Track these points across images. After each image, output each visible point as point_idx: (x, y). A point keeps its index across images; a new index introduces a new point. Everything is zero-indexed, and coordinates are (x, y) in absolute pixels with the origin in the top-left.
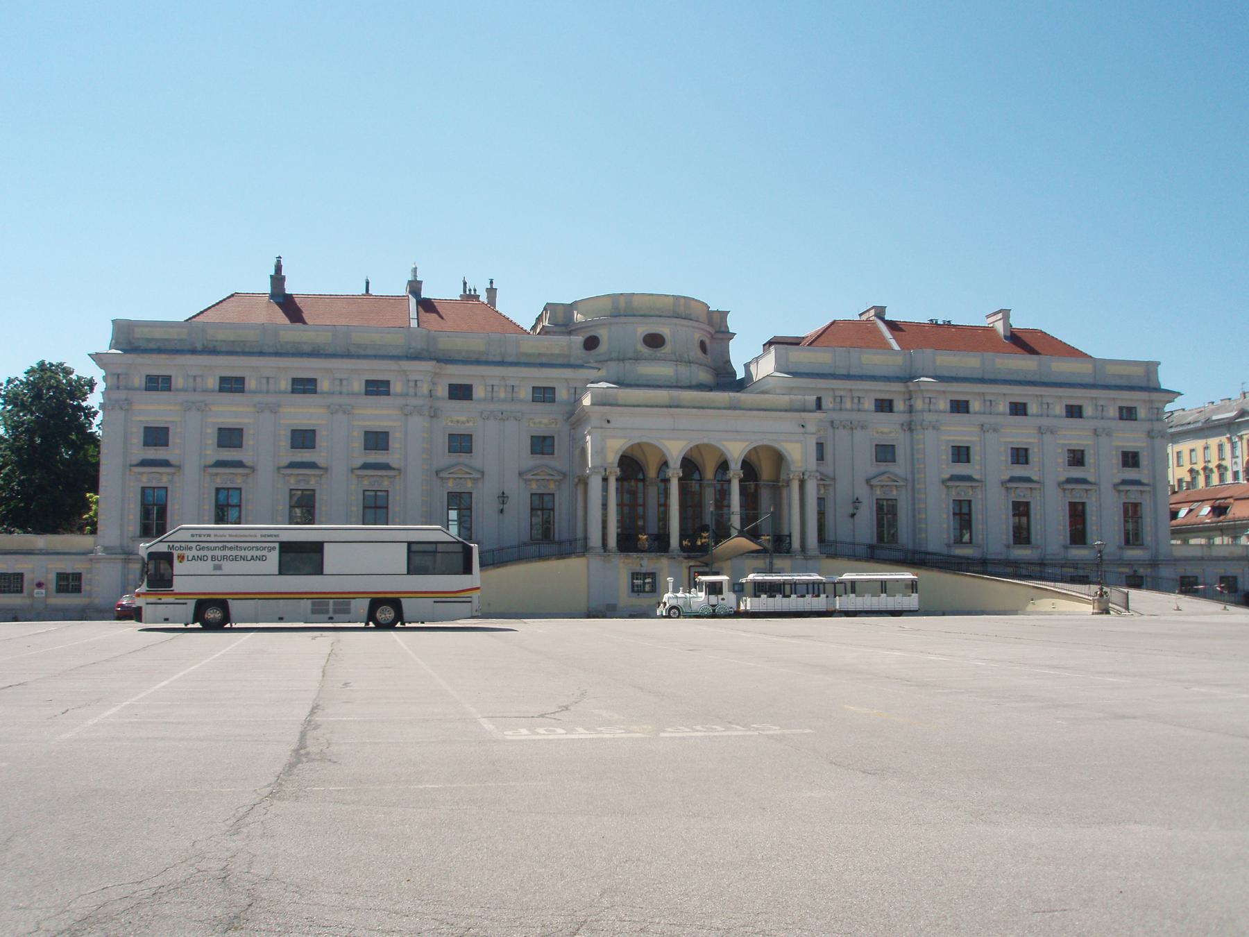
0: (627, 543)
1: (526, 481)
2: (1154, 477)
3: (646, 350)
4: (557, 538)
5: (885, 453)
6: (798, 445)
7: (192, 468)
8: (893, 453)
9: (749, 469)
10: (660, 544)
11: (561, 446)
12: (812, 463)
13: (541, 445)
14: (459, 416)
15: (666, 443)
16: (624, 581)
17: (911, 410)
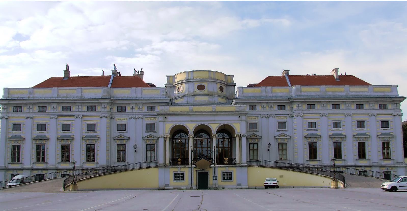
0: (174, 162)
5: (282, 126)
6: (239, 125)
10: (185, 162)
16: (172, 176)
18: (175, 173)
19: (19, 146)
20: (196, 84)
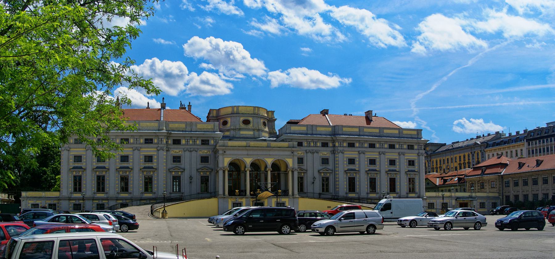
0: (232, 193)
3: (243, 126)
5: (325, 161)
7: (136, 169)
8: (328, 161)
9: (275, 166)
10: (243, 193)
11: (211, 160)
12: (296, 166)
13: (204, 159)
14: (176, 151)
15: (266, 159)
17: (334, 146)
19: (80, 177)
20: (242, 119)
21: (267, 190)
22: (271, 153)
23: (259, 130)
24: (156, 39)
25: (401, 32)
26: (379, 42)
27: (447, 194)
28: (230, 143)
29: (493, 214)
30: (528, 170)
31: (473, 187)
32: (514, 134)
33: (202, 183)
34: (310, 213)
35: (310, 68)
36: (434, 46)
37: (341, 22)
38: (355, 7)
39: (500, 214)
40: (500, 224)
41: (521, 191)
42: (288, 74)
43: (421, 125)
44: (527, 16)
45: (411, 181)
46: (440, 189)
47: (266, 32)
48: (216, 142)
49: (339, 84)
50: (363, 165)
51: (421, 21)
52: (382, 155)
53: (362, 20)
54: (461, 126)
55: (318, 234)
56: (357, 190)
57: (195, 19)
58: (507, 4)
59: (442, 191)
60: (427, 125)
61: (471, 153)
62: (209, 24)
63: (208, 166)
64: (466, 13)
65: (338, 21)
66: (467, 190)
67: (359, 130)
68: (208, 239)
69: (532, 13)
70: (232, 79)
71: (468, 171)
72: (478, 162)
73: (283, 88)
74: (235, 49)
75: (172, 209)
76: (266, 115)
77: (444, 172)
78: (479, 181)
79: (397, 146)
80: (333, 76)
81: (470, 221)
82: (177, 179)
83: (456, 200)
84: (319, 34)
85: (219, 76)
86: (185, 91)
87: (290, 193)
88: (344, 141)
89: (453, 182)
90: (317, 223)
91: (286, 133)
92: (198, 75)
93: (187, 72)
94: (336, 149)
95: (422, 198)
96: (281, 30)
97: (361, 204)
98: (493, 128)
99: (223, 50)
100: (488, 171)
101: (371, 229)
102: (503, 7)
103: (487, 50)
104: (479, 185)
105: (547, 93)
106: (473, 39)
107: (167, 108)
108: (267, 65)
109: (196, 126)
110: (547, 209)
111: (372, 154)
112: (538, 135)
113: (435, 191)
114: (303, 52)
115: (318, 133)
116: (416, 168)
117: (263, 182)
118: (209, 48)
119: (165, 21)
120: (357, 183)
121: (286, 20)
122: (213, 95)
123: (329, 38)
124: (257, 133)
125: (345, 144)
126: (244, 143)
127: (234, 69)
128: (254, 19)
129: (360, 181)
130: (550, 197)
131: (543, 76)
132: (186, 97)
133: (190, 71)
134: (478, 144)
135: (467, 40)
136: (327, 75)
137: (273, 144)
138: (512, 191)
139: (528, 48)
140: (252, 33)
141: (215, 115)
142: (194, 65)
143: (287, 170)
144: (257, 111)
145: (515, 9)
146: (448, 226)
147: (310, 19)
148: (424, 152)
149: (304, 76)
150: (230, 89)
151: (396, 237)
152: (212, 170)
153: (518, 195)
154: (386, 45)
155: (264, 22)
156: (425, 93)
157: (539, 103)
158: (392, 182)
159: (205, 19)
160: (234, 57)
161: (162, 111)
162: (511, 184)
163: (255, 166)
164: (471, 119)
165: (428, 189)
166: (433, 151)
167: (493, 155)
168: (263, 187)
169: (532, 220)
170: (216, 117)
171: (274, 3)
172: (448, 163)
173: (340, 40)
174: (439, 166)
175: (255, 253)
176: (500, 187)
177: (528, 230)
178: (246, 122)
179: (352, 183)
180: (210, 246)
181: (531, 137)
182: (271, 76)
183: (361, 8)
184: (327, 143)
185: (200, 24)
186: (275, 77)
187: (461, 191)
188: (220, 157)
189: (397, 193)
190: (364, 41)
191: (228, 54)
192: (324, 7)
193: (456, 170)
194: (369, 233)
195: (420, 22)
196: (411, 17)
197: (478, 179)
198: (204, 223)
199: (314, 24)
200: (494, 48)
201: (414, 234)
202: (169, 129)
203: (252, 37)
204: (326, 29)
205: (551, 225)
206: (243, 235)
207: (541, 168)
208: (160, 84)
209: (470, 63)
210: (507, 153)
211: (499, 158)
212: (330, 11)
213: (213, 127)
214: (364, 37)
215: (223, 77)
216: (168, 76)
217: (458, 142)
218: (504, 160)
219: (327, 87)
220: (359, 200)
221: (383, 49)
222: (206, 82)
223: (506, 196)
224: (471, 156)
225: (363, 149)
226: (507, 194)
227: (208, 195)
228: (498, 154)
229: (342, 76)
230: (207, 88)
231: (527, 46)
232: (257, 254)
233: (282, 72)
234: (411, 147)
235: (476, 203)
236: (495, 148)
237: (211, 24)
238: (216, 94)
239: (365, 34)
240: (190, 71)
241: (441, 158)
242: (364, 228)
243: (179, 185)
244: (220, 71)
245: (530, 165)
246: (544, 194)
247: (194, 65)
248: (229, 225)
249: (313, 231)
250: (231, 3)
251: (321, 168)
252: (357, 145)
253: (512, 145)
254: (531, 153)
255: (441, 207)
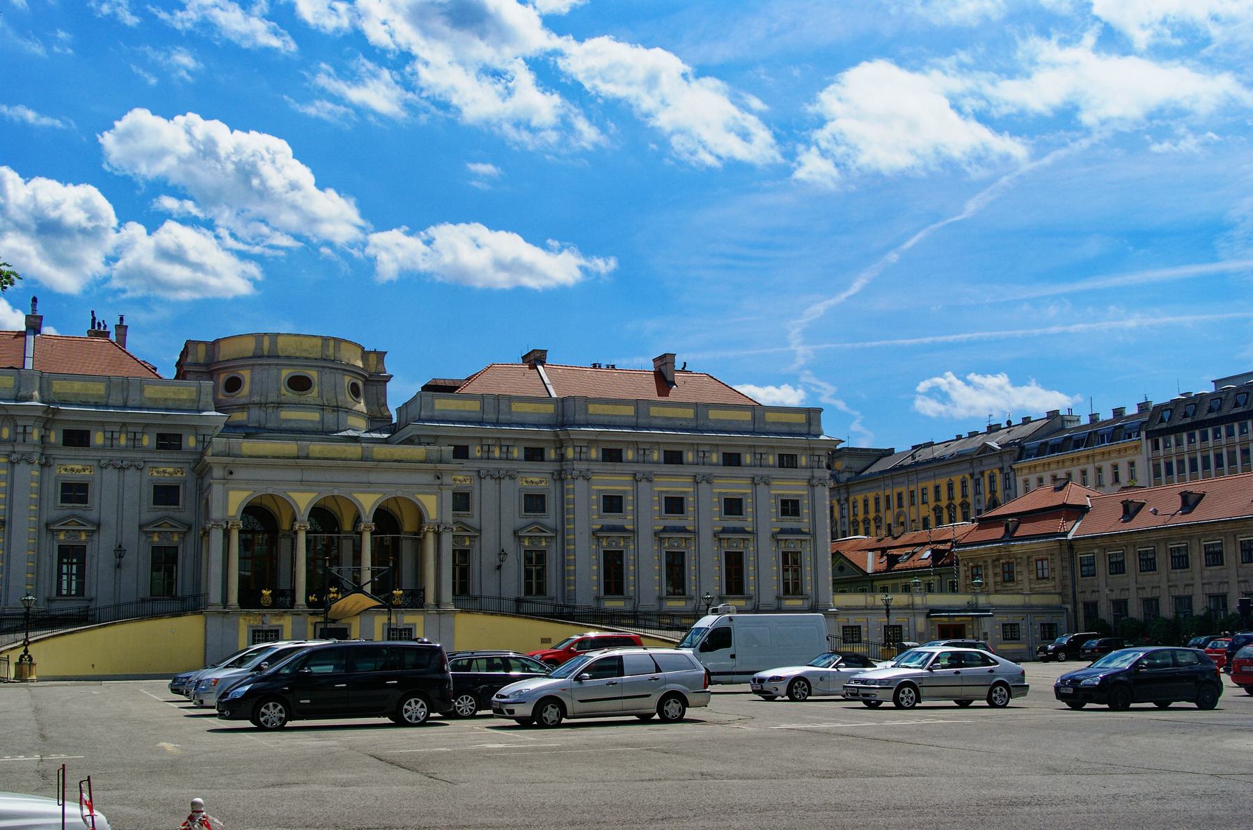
0: (249, 599)
1: (146, 533)
2: (814, 526)
3: (289, 395)
4: (179, 594)
5: (534, 503)
6: (434, 497)
9: (385, 518)
10: (283, 601)
12: (449, 517)
13: (165, 494)
14: (73, 467)
17: (562, 458)
18: (254, 631)
20: (286, 373)
21: (359, 590)
22: (373, 477)
23: (337, 409)
24: (9, 105)
25: (765, 119)
26: (701, 150)
27: (900, 599)
28: (249, 446)
29: (1045, 660)
30: (1157, 522)
31: (980, 576)
32: (1131, 410)
33: (155, 567)
34: (490, 660)
35: (494, 226)
36: (863, 160)
37: (588, 86)
38: (633, 42)
39: (1067, 659)
40: (1070, 691)
41: (1133, 586)
42: (429, 242)
43: (820, 395)
44: (1160, 53)
45: (791, 561)
46: (878, 584)
47: (362, 111)
48: (205, 443)
49: (578, 274)
50: (646, 514)
51: (827, 85)
52: (703, 485)
53: (652, 81)
54: (941, 396)
55: (514, 722)
56: (630, 589)
57: (137, 52)
58: (1097, 19)
59: (884, 590)
60: (837, 396)
61: (972, 475)
62: (184, 73)
63: (177, 515)
64: (964, 56)
65: (580, 85)
66: (961, 586)
67: (637, 410)
68: (169, 746)
69: (1178, 42)
70: (257, 250)
71: (962, 529)
72: (994, 504)
73: (413, 283)
74: (267, 156)
75: (52, 650)
76: (360, 364)
77: (890, 533)
78: (998, 559)
79: (747, 459)
80: (560, 251)
81: (975, 681)
82: (72, 554)
83: (928, 616)
84: (522, 124)
85: (217, 237)
86: (107, 279)
87: (430, 598)
88: (591, 443)
89: (918, 564)
90: (508, 689)
91: (420, 420)
92: (149, 233)
93: (114, 221)
94: (567, 466)
95: (824, 611)
96: (407, 105)
97: (640, 631)
98: (1040, 401)
99: (228, 157)
100: (1024, 530)
101: (671, 706)
102: (1084, 30)
103: (1027, 167)
104: (999, 570)
105: (1220, 290)
106: (983, 134)
107: (48, 330)
108: (366, 210)
109: (142, 391)
110: (1223, 643)
111: (675, 482)
112: (1185, 416)
113: (863, 591)
114: (475, 176)
115: (515, 419)
116: (804, 523)
117: (347, 565)
118: (186, 149)
119: (38, 50)
120: (629, 568)
121: (426, 76)
122: (196, 296)
123: (553, 137)
124: (330, 417)
125: (594, 454)
126: (290, 447)
127: (263, 221)
128: (323, 66)
129: (637, 563)
130: (1233, 606)
131: (1206, 236)
132: (110, 300)
133: (123, 219)
134: (993, 449)
135: (964, 137)
136: (545, 247)
137: (381, 451)
138: (1104, 590)
139: (1157, 154)
140: (318, 109)
141: (201, 361)
142: (136, 199)
143: (420, 528)
144: (331, 350)
145: (1120, 34)
146: (906, 695)
147: (495, 74)
148: (827, 473)
149: (474, 250)
150: (252, 279)
151: (748, 729)
152: (190, 528)
153: (1125, 602)
154: (719, 158)
155: (354, 78)
156: (832, 302)
157: (1188, 319)
158: (734, 564)
159: (169, 55)
160: (263, 183)
161: (30, 338)
162: (1102, 568)
163: (323, 516)
164: (972, 377)
165: (841, 585)
166: (855, 470)
167: (1041, 480)
168: (347, 580)
169: (1174, 678)
170: (206, 365)
171: (390, 16)
172: (900, 506)
173: (584, 144)
174: (872, 515)
175: (317, 787)
176: (1064, 578)
177: (1163, 706)
178: (300, 384)
179: (614, 573)
180: (174, 767)
181: (1164, 425)
182: (376, 246)
183: (648, 44)
184: (542, 450)
185: (155, 69)
186: (387, 250)
187: (941, 591)
188: (217, 490)
189: (750, 598)
190: (653, 146)
191: (247, 171)
192: (540, 40)
193: (926, 525)
194: (665, 720)
195: (824, 86)
196: (796, 72)
197: (995, 553)
198: (155, 697)
199: (509, 92)
200: (1047, 161)
201: (803, 721)
202: (53, 397)
203: (318, 121)
204: (545, 107)
205: (1243, 691)
206: (282, 728)
207: (1196, 516)
208: (21, 254)
209: (971, 207)
210: (1084, 473)
211: (1061, 489)
212: (557, 53)
213: (194, 396)
214: (655, 134)
215: (230, 242)
216: (48, 229)
217: (931, 444)
218: (1075, 495)
219: (544, 283)
220: (636, 618)
221: (710, 170)
222: (175, 256)
223: (1086, 605)
224: (970, 484)
225: (647, 468)
226: (1090, 598)
227: (176, 606)
228: (1055, 478)
229: (587, 250)
230: (178, 273)
231: (1156, 148)
232: (324, 789)
233: (409, 234)
234: (787, 461)
235: (990, 626)
236: (1045, 459)
237: (189, 72)
238: (209, 295)
239: (658, 124)
240: (123, 219)
241: (881, 493)
242: (650, 704)
243: (81, 574)
244: (219, 222)
245: (1162, 508)
246: (1210, 596)
247: (136, 199)
248: (235, 700)
249: (499, 712)
250: (256, 10)
251: (524, 522)
252: (629, 454)
253: (1099, 449)
254: (1163, 472)
255: (881, 639)
